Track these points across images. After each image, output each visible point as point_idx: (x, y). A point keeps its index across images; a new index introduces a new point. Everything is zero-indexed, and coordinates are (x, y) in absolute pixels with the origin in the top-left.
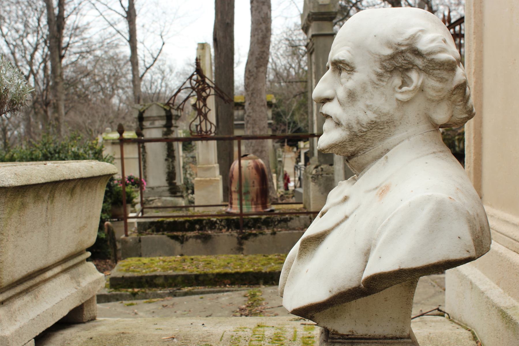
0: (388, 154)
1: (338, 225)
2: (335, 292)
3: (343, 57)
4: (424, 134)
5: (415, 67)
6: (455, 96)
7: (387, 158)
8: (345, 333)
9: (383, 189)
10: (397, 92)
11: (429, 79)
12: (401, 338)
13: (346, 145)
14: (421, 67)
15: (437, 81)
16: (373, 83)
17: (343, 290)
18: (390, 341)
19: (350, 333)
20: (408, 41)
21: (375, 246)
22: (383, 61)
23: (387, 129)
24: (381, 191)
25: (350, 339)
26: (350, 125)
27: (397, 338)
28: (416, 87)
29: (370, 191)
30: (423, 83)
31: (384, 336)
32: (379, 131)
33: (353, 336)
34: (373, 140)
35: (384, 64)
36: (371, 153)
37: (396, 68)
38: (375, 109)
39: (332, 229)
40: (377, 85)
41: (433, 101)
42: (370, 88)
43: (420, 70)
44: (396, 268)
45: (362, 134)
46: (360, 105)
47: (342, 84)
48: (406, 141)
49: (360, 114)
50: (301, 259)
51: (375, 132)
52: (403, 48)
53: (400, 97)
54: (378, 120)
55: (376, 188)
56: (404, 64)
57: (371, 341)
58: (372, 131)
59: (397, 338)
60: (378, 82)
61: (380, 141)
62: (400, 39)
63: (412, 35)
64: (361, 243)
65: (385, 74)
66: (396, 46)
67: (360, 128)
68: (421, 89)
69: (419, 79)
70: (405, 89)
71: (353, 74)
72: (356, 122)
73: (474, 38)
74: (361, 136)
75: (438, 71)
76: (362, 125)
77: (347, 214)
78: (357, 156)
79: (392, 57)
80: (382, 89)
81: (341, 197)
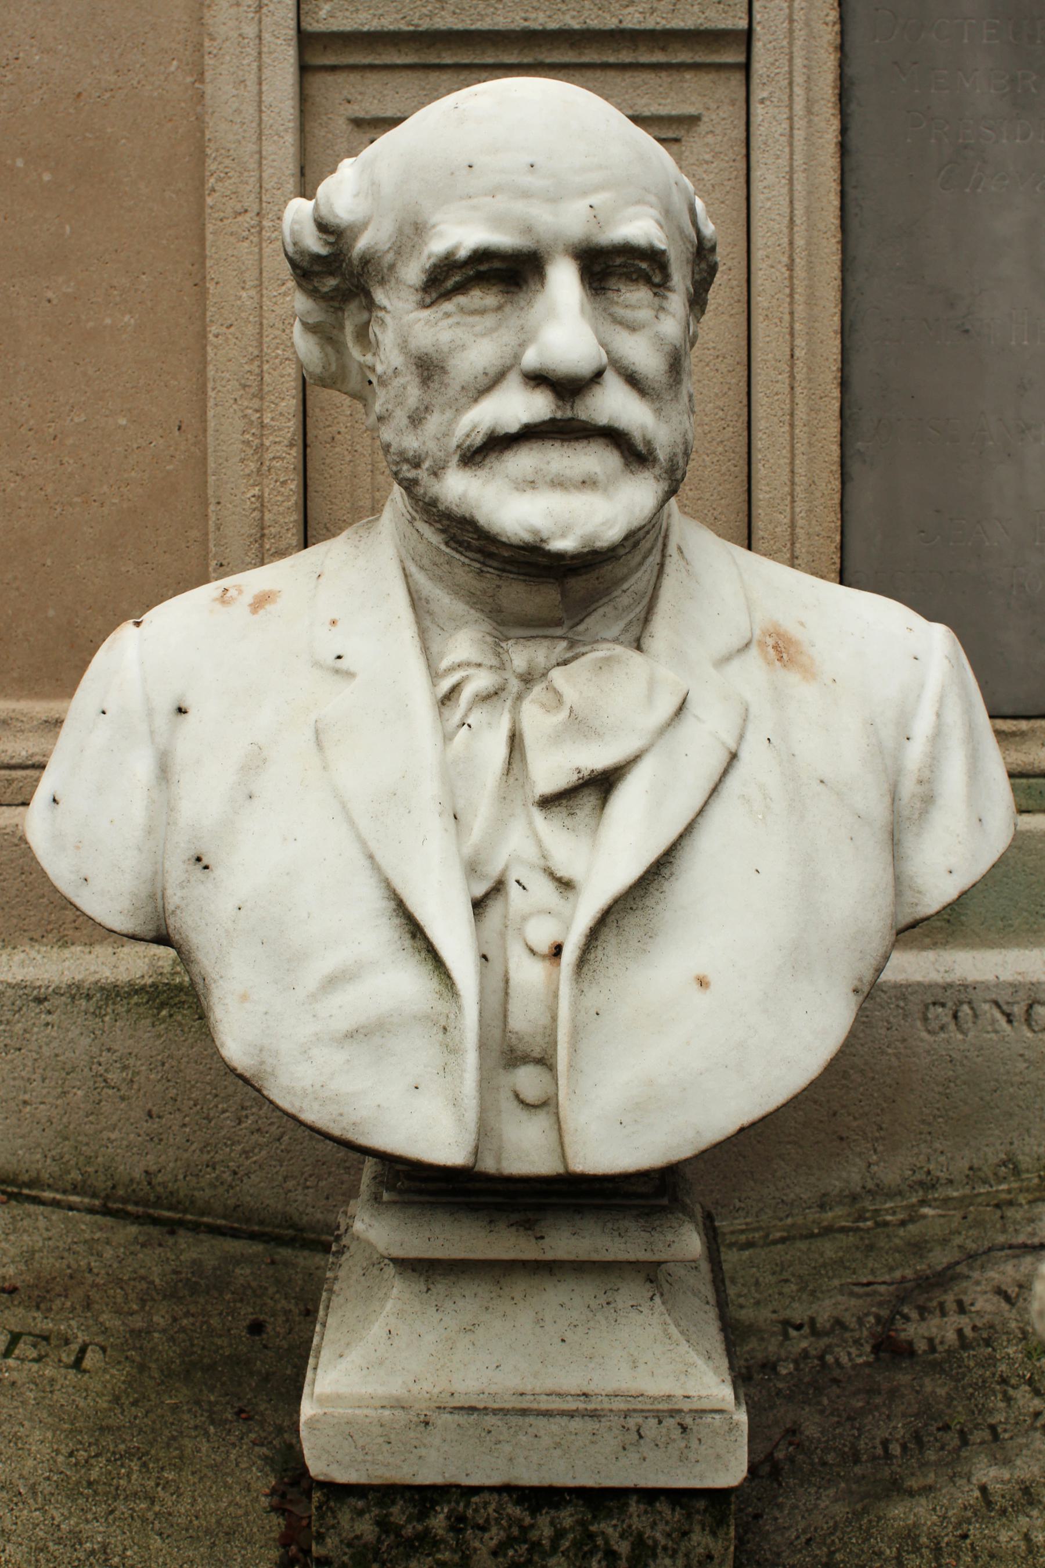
47: (632, 328)
55: (747, 645)
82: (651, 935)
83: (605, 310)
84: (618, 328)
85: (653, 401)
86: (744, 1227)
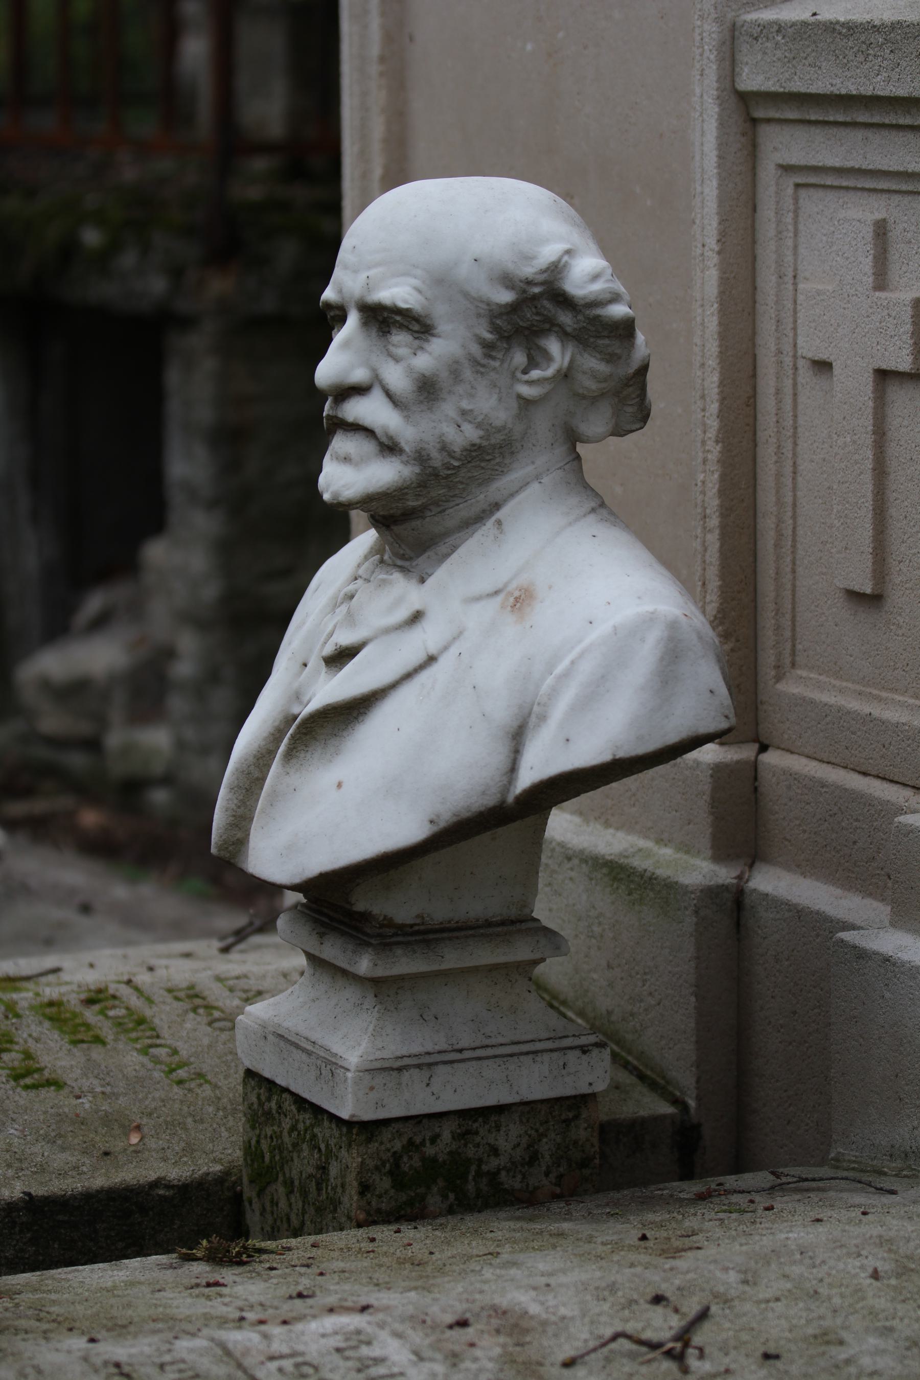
0: (499, 515)
1: (408, 676)
2: (446, 818)
3: (406, 302)
4: (567, 467)
5: (556, 329)
6: (631, 389)
7: (499, 523)
8: (409, 922)
9: (517, 594)
10: (519, 381)
11: (586, 355)
12: (521, 921)
13: (407, 494)
14: (569, 329)
15: (602, 360)
16: (475, 362)
17: (466, 815)
18: (499, 929)
19: (418, 921)
20: (545, 275)
21: (543, 718)
22: (496, 317)
23: (498, 460)
24: (512, 600)
25: (418, 933)
26: (423, 453)
27: (513, 922)
28: (559, 371)
29: (478, 599)
30: (572, 361)
31: (486, 920)
32: (483, 464)
33: (422, 928)
34: (467, 484)
35: (498, 322)
36: (463, 510)
37: (518, 331)
38: (479, 419)
39: (394, 686)
40: (483, 366)
41: (584, 397)
42: (468, 373)
43: (565, 336)
44: (606, 757)
45: (449, 472)
46: (449, 408)
47: (397, 360)
48: (535, 487)
49: (445, 428)
50: (294, 761)
51: (475, 467)
52: (537, 290)
53: (526, 391)
54: (485, 443)
55: (497, 593)
56: (535, 323)
57: (463, 933)
58: (469, 465)
59: (513, 922)
60: (484, 361)
61: (480, 485)
62: (528, 271)
63: (553, 263)
64: (502, 712)
65: (499, 344)
66: (522, 284)
67: (447, 459)
68: (565, 375)
69: (563, 354)
70: (535, 374)
71: (427, 341)
72: (438, 446)
73: (381, 74)
74: (448, 476)
75: (607, 341)
76: (451, 454)
77: (433, 650)
78: (424, 518)
79: (513, 308)
80: (493, 375)
81: (403, 613)
82: (337, 753)
83: (385, 346)
84: (390, 359)
85: (402, 410)
86: (854, 1159)
